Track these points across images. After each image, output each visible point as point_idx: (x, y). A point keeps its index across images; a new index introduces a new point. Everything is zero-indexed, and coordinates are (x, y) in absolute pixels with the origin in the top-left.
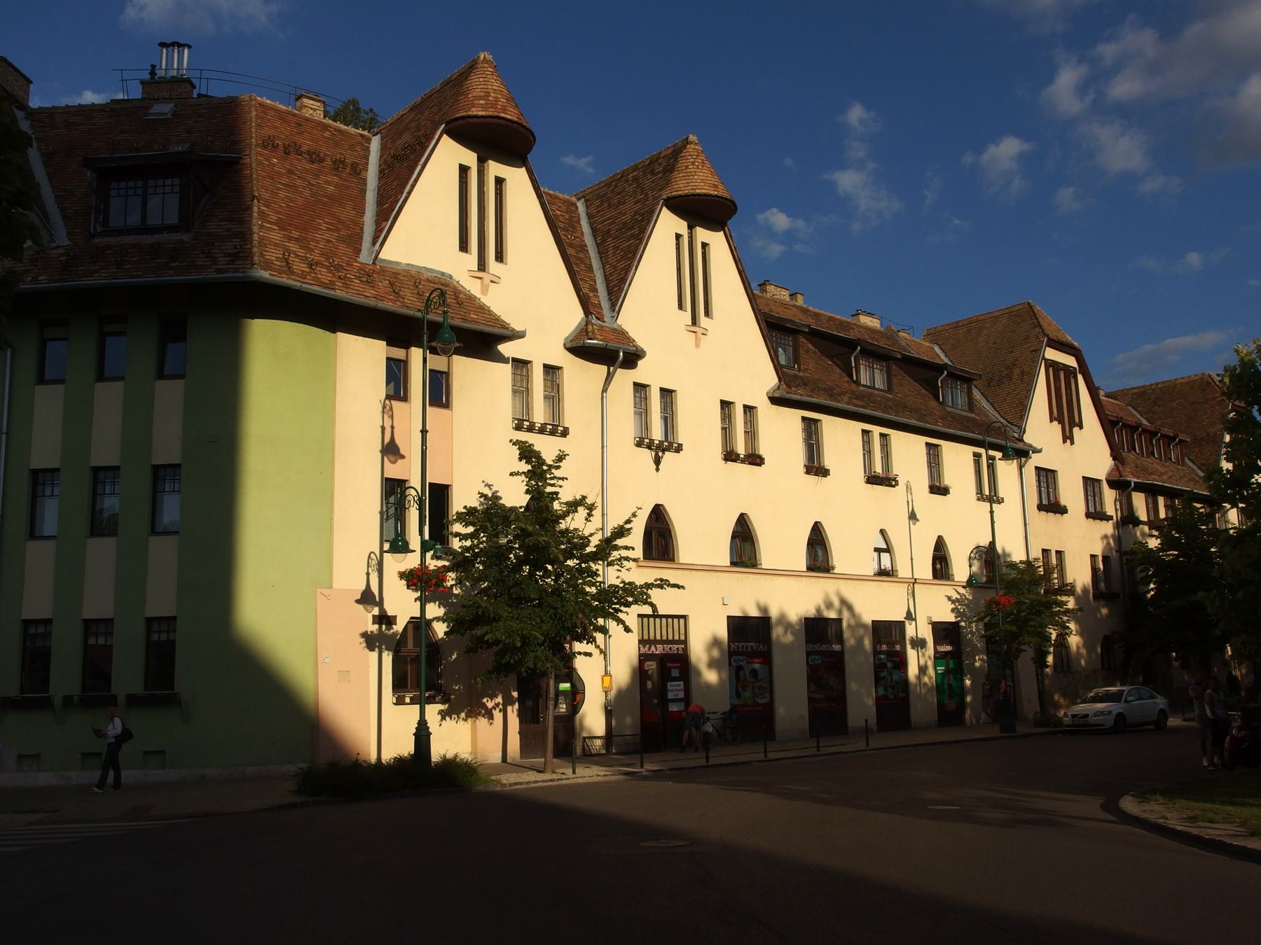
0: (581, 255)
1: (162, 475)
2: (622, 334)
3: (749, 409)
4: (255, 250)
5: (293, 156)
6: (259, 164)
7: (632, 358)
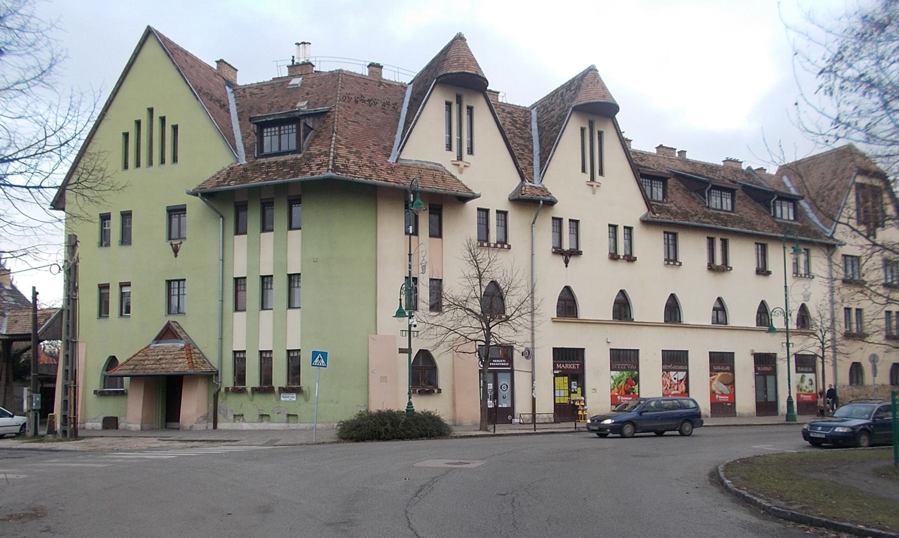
0: (527, 143)
2: (544, 190)
3: (629, 230)
5: (360, 103)
7: (551, 203)
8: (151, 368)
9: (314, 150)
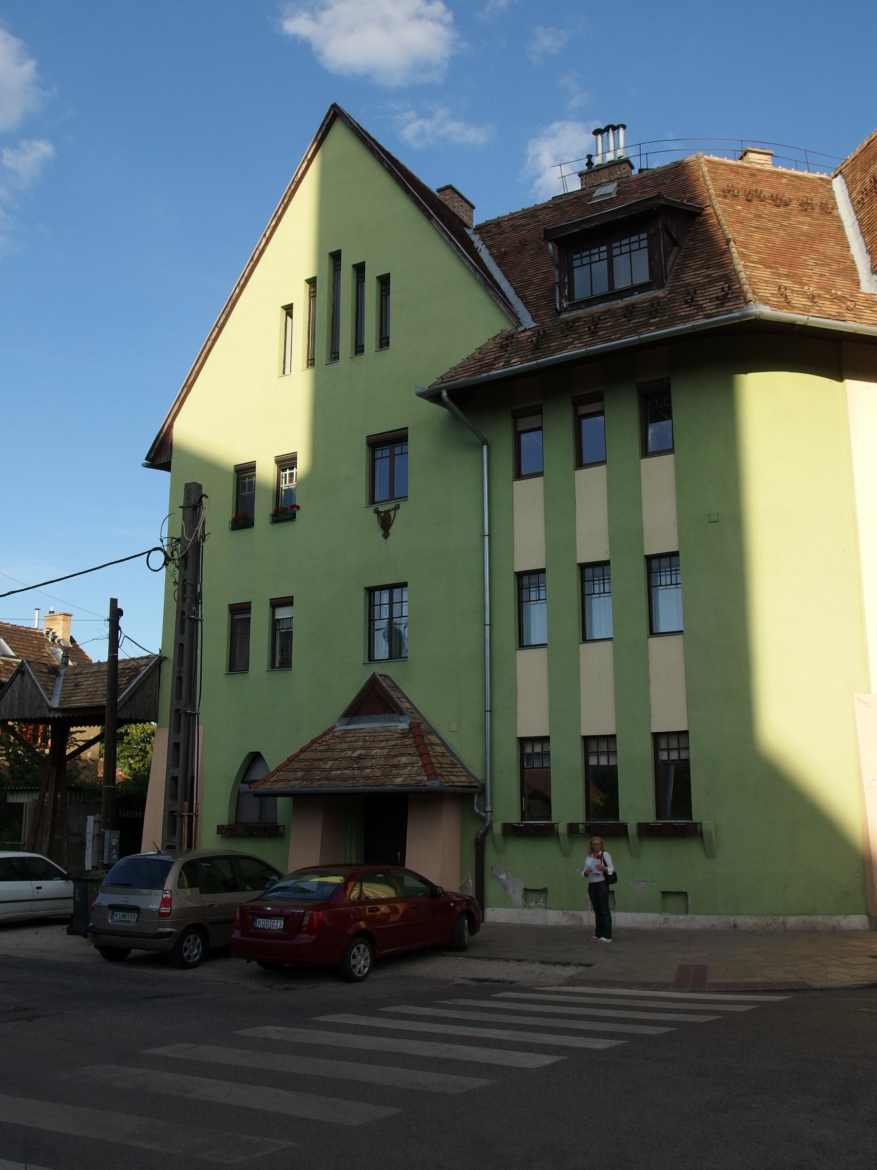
1: (658, 566)
4: (746, 287)
5: (755, 202)
6: (723, 213)
8: (339, 777)
9: (689, 277)
